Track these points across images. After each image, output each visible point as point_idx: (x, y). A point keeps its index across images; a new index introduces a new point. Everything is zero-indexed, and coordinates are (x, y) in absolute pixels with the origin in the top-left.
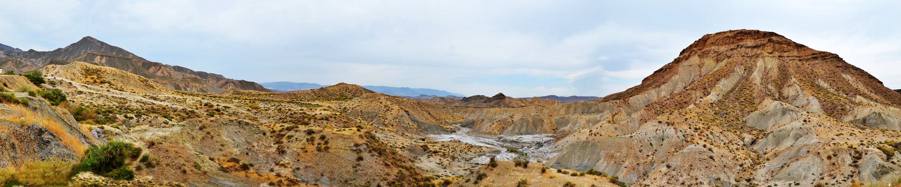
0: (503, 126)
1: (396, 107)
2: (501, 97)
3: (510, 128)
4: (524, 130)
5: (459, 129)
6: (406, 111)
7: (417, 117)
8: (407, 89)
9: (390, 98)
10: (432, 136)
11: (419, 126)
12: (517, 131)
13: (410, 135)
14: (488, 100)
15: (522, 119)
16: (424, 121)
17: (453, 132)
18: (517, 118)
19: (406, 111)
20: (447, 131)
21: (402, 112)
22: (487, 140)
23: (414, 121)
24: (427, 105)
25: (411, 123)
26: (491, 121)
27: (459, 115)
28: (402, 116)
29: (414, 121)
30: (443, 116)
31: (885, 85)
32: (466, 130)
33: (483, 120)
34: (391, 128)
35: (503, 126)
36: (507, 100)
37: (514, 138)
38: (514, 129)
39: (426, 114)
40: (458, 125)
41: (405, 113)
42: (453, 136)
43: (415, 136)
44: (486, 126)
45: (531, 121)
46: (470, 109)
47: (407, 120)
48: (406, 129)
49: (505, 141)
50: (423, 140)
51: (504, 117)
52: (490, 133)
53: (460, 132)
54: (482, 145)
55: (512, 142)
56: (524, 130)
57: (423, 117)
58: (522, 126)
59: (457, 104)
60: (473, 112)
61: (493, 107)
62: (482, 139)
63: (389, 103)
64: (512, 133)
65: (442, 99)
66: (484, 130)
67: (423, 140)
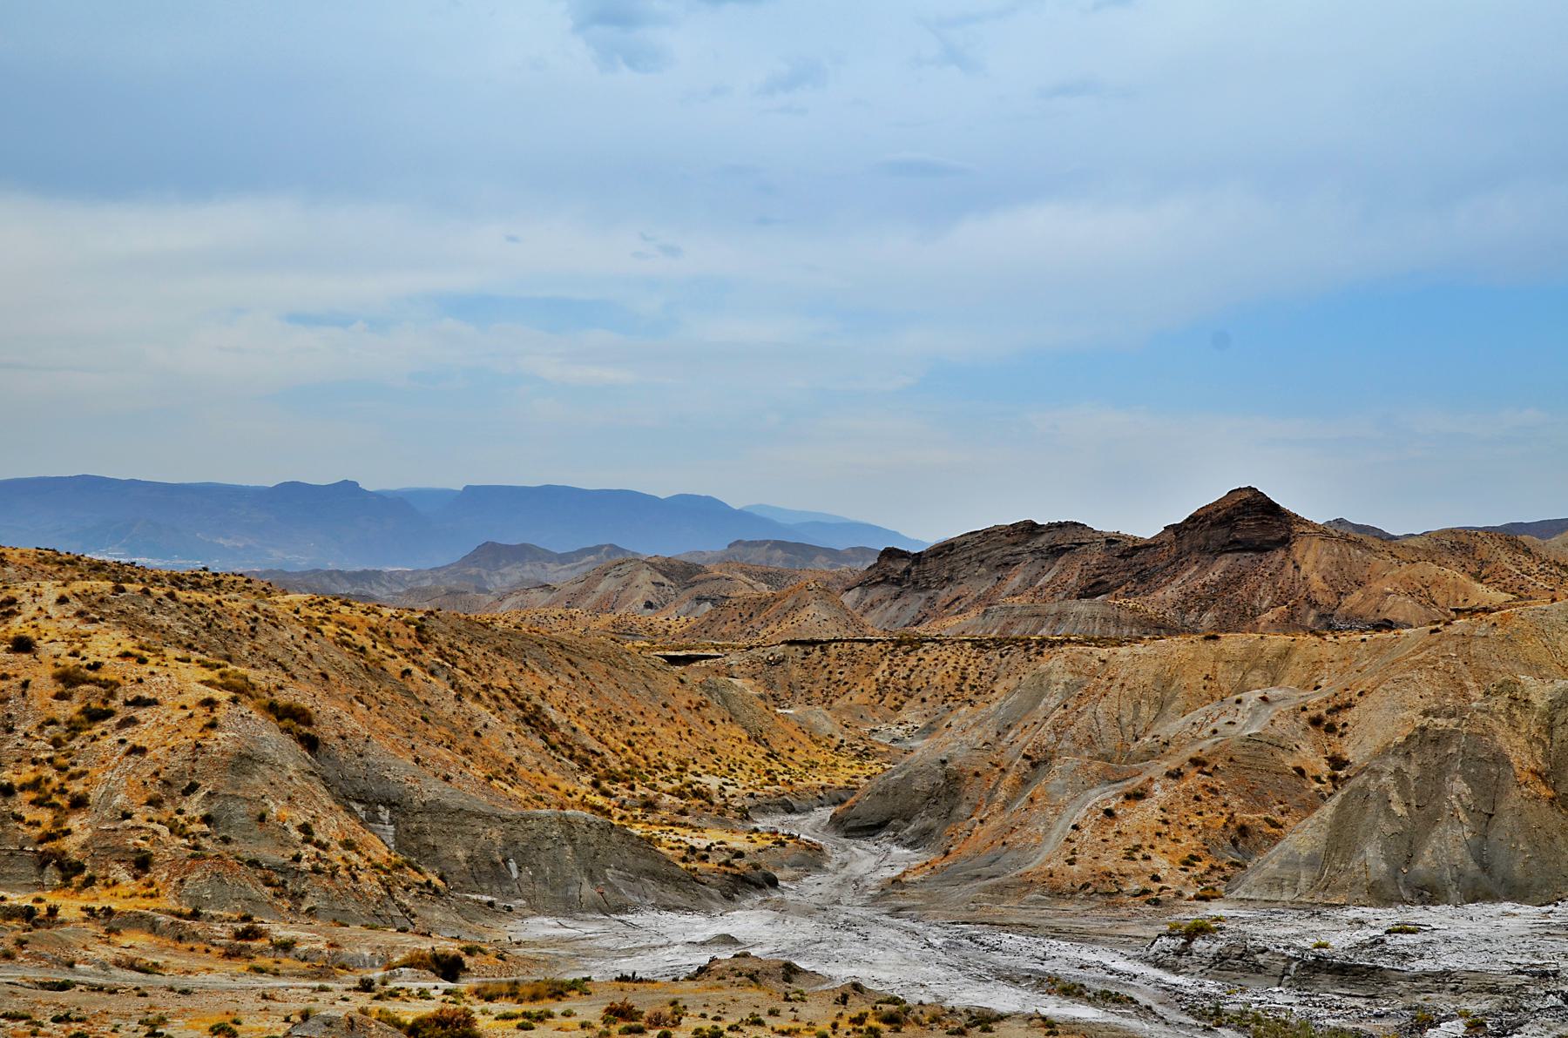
0: (1241, 809)
1: (184, 680)
2: (1248, 525)
3: (1304, 836)
4: (1447, 847)
5: (812, 859)
6: (291, 717)
7: (395, 763)
8: (340, 502)
9: (115, 591)
10: (542, 927)
11: (414, 848)
12: (1373, 858)
13: (310, 937)
14: (1121, 566)
15: (1423, 739)
16: (467, 788)
17: (746, 882)
18: (1374, 729)
19: (291, 717)
20: (684, 884)
21: (244, 727)
22: (1064, 957)
23: (366, 798)
24: (515, 645)
25: (332, 826)
26: (1117, 764)
27: (823, 720)
28: (244, 762)
29: (366, 798)
30: (667, 742)
31: (368, 485)
32: (877, 861)
33: (1038, 762)
34: (123, 892)
35: (1241, 809)
36: (1312, 564)
37: (1339, 935)
38: (1341, 840)
39: (501, 732)
40: (809, 826)
41: (272, 738)
42: (753, 926)
43: (361, 942)
44: (1063, 825)
45: (1522, 754)
46: (937, 666)
47: (294, 801)
48: (284, 883)
49: (1242, 962)
50: (449, 968)
51: (1248, 722)
52: (1104, 890)
53: (815, 887)
54: (1004, 999)
55: (1316, 969)
56: (1447, 847)
57: (473, 767)
58: (1427, 810)
59: (815, 620)
60: (966, 690)
61: (1160, 628)
62: (1016, 949)
63: (106, 643)
64: (1326, 884)
65: (681, 574)
66: (1046, 857)
67: (449, 968)
